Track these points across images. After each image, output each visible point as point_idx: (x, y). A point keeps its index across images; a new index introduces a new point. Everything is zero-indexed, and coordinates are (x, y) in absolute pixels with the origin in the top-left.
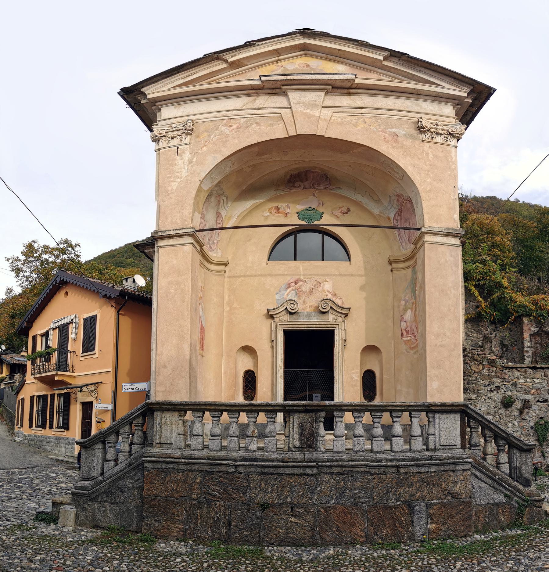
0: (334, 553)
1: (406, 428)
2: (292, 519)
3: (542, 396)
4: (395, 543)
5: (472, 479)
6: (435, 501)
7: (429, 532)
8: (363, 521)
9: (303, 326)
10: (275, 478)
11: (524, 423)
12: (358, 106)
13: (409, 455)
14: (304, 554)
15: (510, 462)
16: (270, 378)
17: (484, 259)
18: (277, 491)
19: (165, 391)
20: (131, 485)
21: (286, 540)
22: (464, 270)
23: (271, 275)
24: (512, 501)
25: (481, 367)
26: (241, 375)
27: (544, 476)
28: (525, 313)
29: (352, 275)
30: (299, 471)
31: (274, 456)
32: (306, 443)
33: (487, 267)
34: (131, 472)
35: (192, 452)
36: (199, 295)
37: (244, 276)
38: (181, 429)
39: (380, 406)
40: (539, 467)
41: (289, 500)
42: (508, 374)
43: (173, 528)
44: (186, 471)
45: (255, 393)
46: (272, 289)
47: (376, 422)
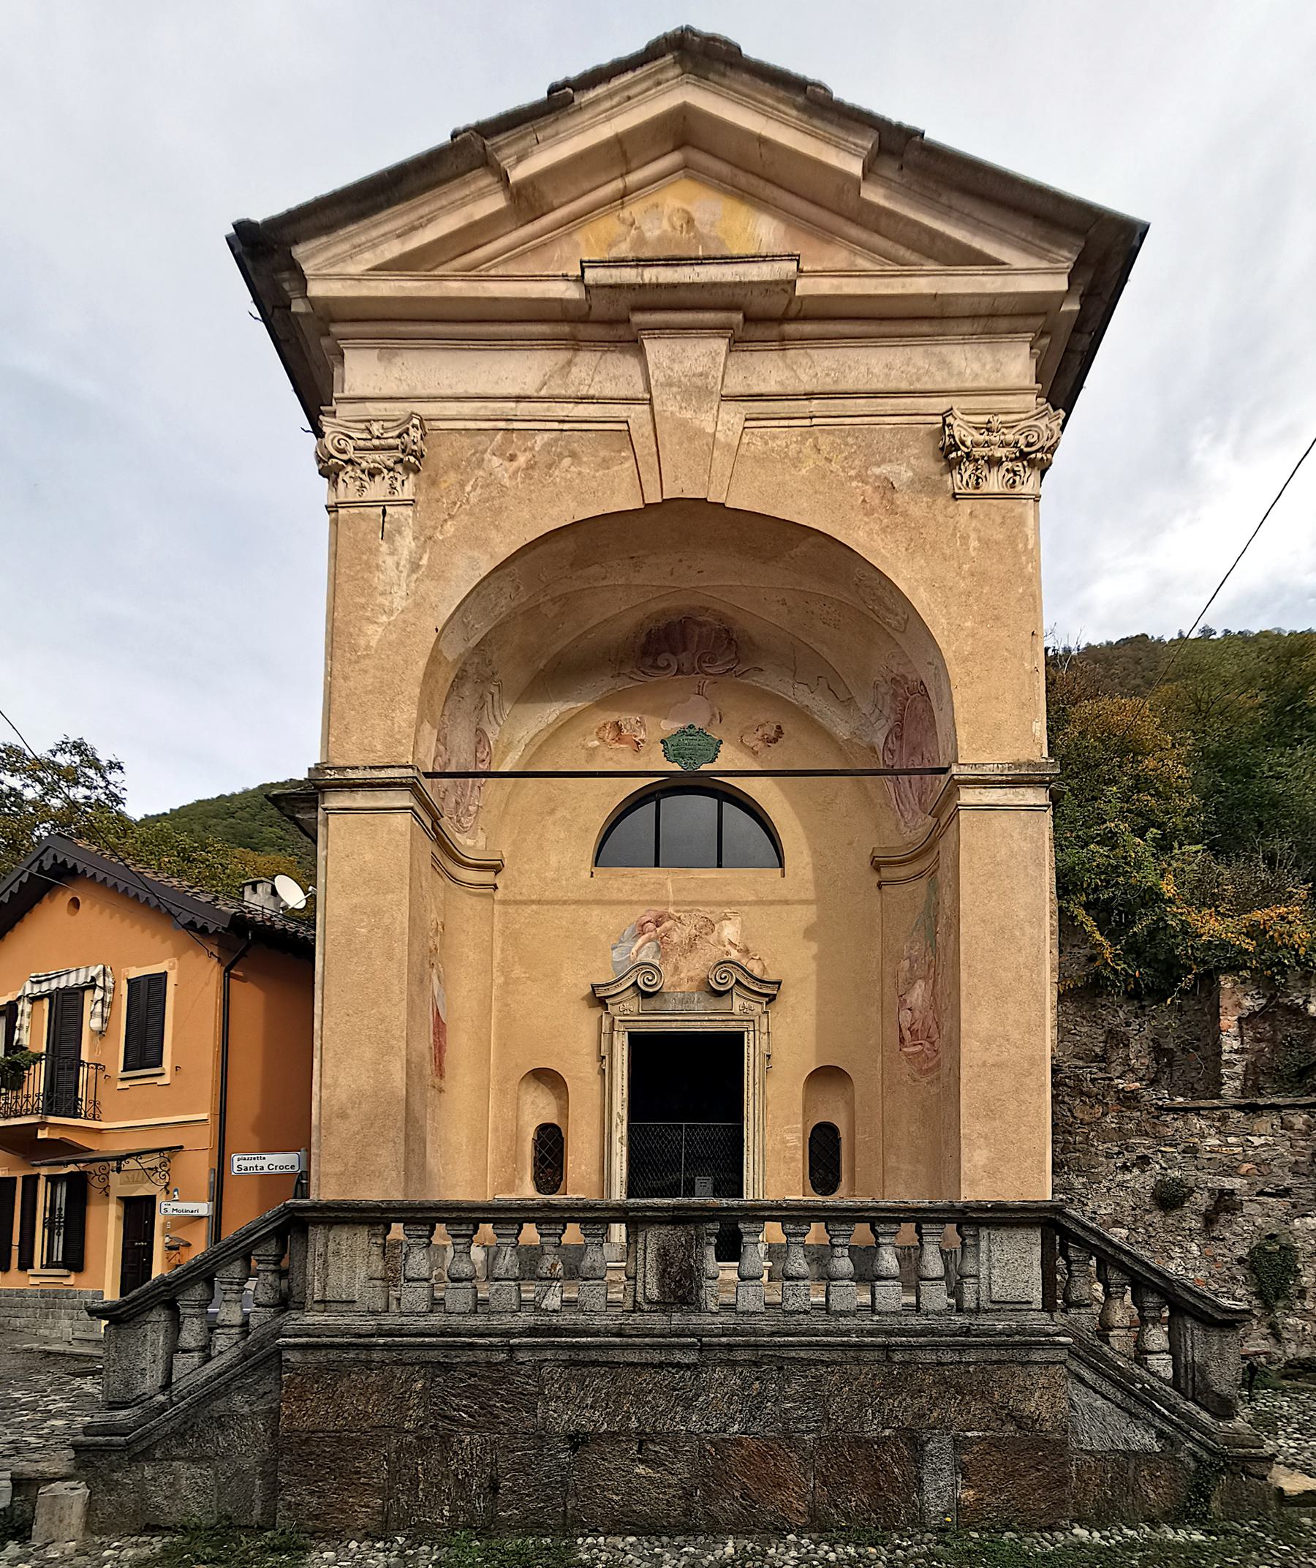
0: (736, 1552)
1: (910, 1255)
2: (640, 1470)
3: (1274, 1180)
4: (876, 1528)
5: (1070, 1385)
6: (976, 1434)
7: (960, 1507)
8: (804, 1475)
9: (674, 1024)
10: (602, 1372)
11: (1216, 1249)
12: (801, 389)
13: (914, 1321)
14: (667, 1556)
15: (1174, 1350)
16: (596, 1142)
17: (1111, 831)
18: (607, 1404)
19: (343, 1174)
20: (246, 1409)
21: (625, 1519)
22: (1057, 868)
23: (599, 902)
24: (1178, 1450)
25: (1099, 1110)
26: (530, 1134)
27: (1275, 1389)
28: (1224, 964)
29: (787, 902)
30: (657, 1357)
31: (600, 1322)
32: (673, 1292)
33: (1120, 852)
34: (247, 1377)
35: (404, 1318)
36: (431, 943)
37: (539, 902)
38: (378, 1266)
39: (847, 1209)
40: (1262, 1365)
41: (634, 1424)
42: (1174, 1125)
43: (356, 1508)
44: (388, 1365)
45: (561, 1174)
46: (603, 937)
47: (838, 1246)
